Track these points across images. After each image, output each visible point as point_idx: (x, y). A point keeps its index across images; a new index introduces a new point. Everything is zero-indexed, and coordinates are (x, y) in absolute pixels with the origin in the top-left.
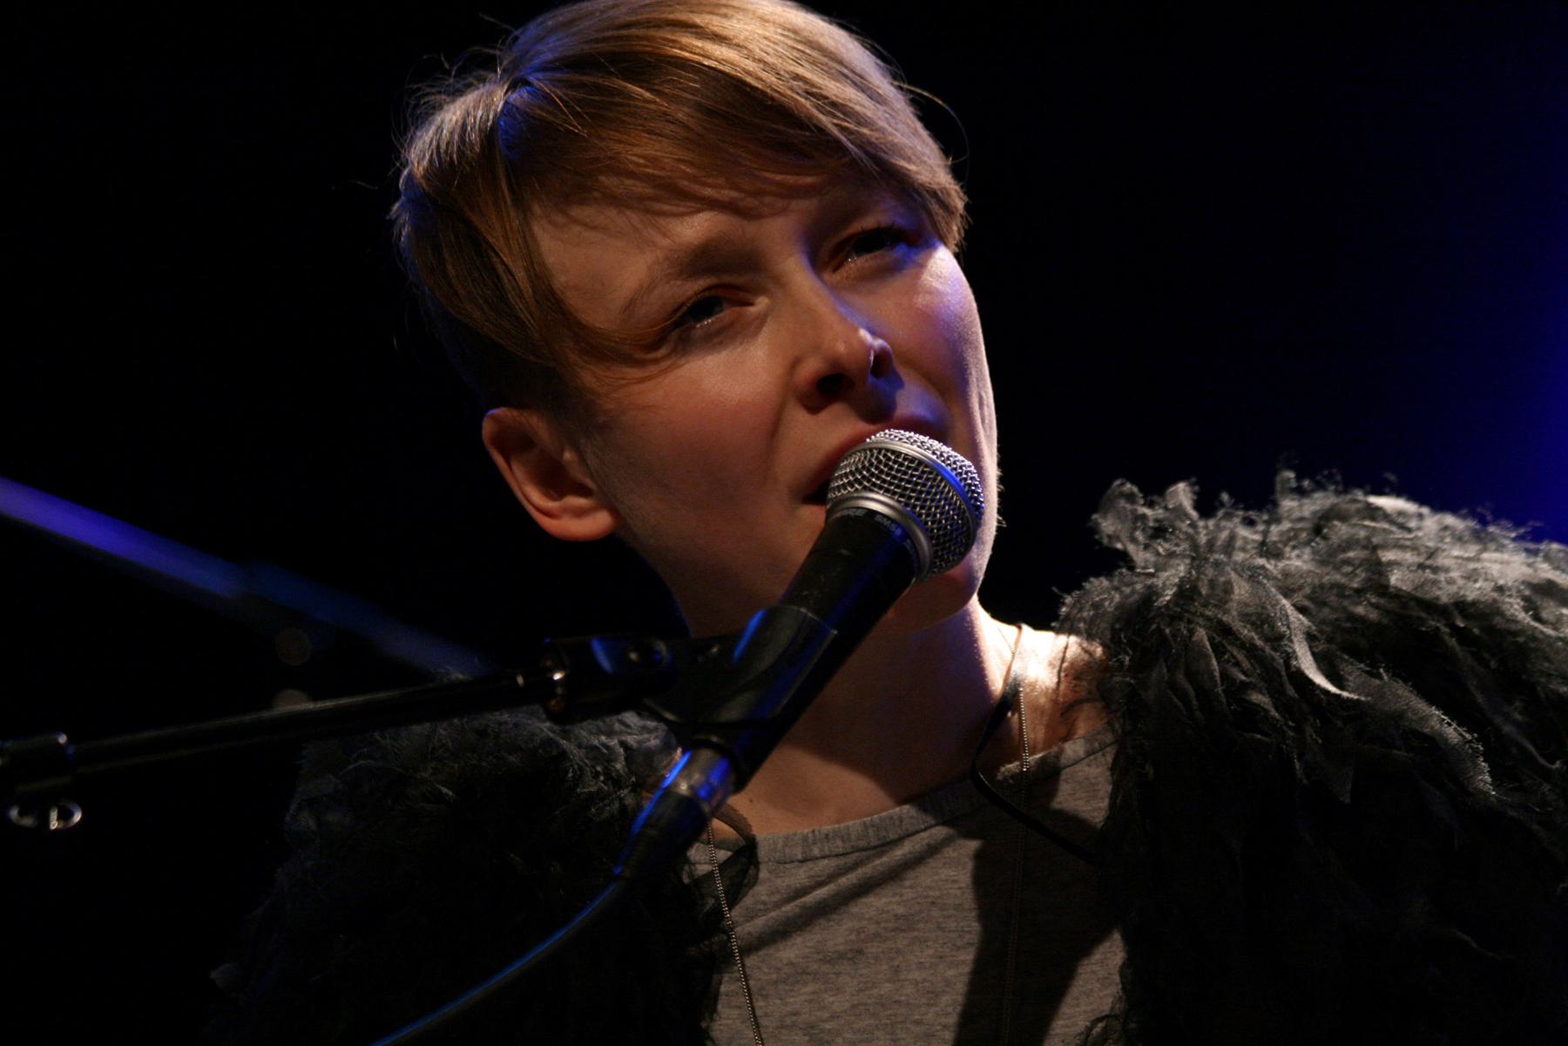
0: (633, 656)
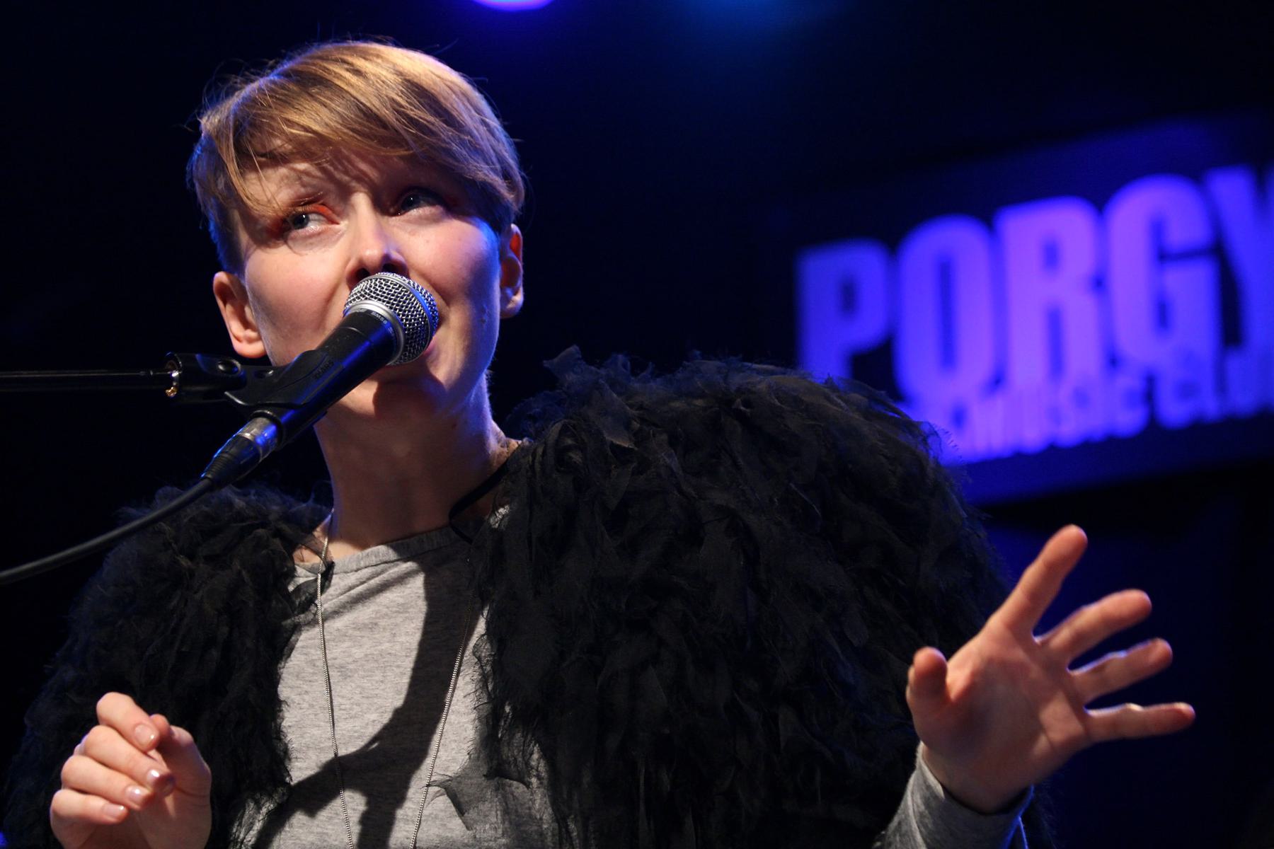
0: (221, 367)
